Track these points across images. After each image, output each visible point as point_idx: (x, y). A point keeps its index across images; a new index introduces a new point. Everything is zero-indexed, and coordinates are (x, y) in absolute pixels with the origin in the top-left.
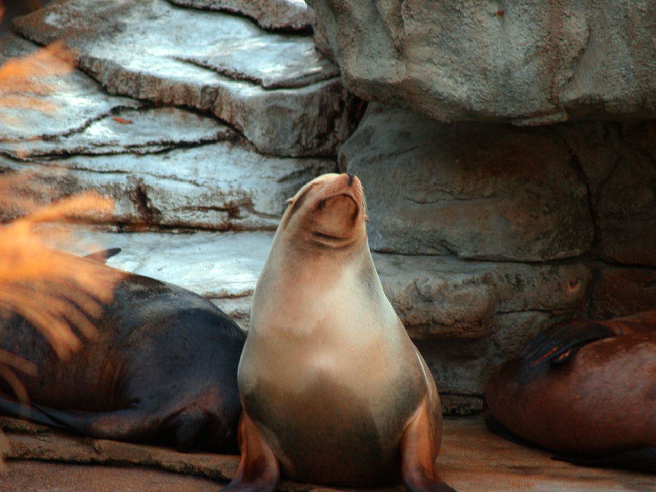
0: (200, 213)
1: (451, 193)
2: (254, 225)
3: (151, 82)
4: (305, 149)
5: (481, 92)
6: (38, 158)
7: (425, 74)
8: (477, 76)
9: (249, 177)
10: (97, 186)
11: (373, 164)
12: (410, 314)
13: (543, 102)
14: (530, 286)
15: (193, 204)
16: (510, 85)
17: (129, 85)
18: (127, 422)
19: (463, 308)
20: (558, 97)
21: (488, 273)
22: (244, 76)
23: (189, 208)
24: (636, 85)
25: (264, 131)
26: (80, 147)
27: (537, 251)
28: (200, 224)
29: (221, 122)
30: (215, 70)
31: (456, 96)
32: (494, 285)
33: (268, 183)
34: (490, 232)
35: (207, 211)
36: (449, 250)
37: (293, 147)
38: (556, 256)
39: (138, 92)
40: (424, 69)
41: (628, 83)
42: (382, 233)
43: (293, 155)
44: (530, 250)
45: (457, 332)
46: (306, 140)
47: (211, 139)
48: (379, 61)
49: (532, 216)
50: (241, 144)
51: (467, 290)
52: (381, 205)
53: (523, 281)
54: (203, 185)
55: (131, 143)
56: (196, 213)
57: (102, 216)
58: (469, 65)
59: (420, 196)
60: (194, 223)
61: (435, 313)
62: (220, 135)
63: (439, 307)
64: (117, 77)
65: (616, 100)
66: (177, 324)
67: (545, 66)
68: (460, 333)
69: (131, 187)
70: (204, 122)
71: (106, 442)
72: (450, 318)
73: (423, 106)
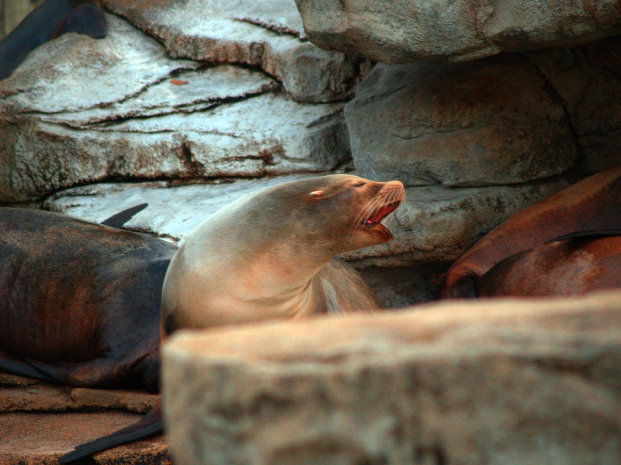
0: (237, 163)
1: (431, 126)
2: (286, 170)
3: (208, 43)
4: (335, 94)
5: (415, 34)
6: (94, 125)
7: (364, 22)
8: (409, 20)
9: (283, 125)
10: (146, 146)
11: (366, 106)
12: (393, 244)
13: (471, 38)
14: (512, 206)
15: (231, 155)
16: (439, 26)
17: (188, 48)
18: (99, 370)
19: (440, 234)
20: (483, 32)
21: (468, 198)
22: (287, 30)
23: (228, 159)
24: (551, 15)
25: (296, 81)
26: (133, 111)
27: (515, 173)
28: (238, 173)
29: (268, 75)
30: (264, 26)
31: (394, 40)
32: (473, 209)
33: (298, 129)
34: (468, 160)
35: (243, 161)
36: (434, 179)
37: (323, 93)
38: (538, 176)
39: (196, 54)
40: (363, 17)
41: (543, 14)
42: (376, 169)
43: (324, 100)
44: (508, 173)
45: (439, 256)
46: (335, 85)
47: (255, 92)
48: (328, 14)
49: (507, 141)
50: (282, 94)
51: (443, 217)
52: (373, 143)
53: (503, 203)
54: (240, 137)
55: (179, 103)
56: (234, 163)
57: (153, 173)
58: (401, 11)
59: (405, 132)
60: (233, 173)
61: (416, 241)
62: (265, 87)
63: (418, 235)
64: (176, 42)
65: (536, 30)
66: (146, 276)
67: (467, 4)
68: (442, 257)
69: (177, 144)
70: (253, 77)
71: (80, 390)
72: (430, 245)
73: (369, 51)
